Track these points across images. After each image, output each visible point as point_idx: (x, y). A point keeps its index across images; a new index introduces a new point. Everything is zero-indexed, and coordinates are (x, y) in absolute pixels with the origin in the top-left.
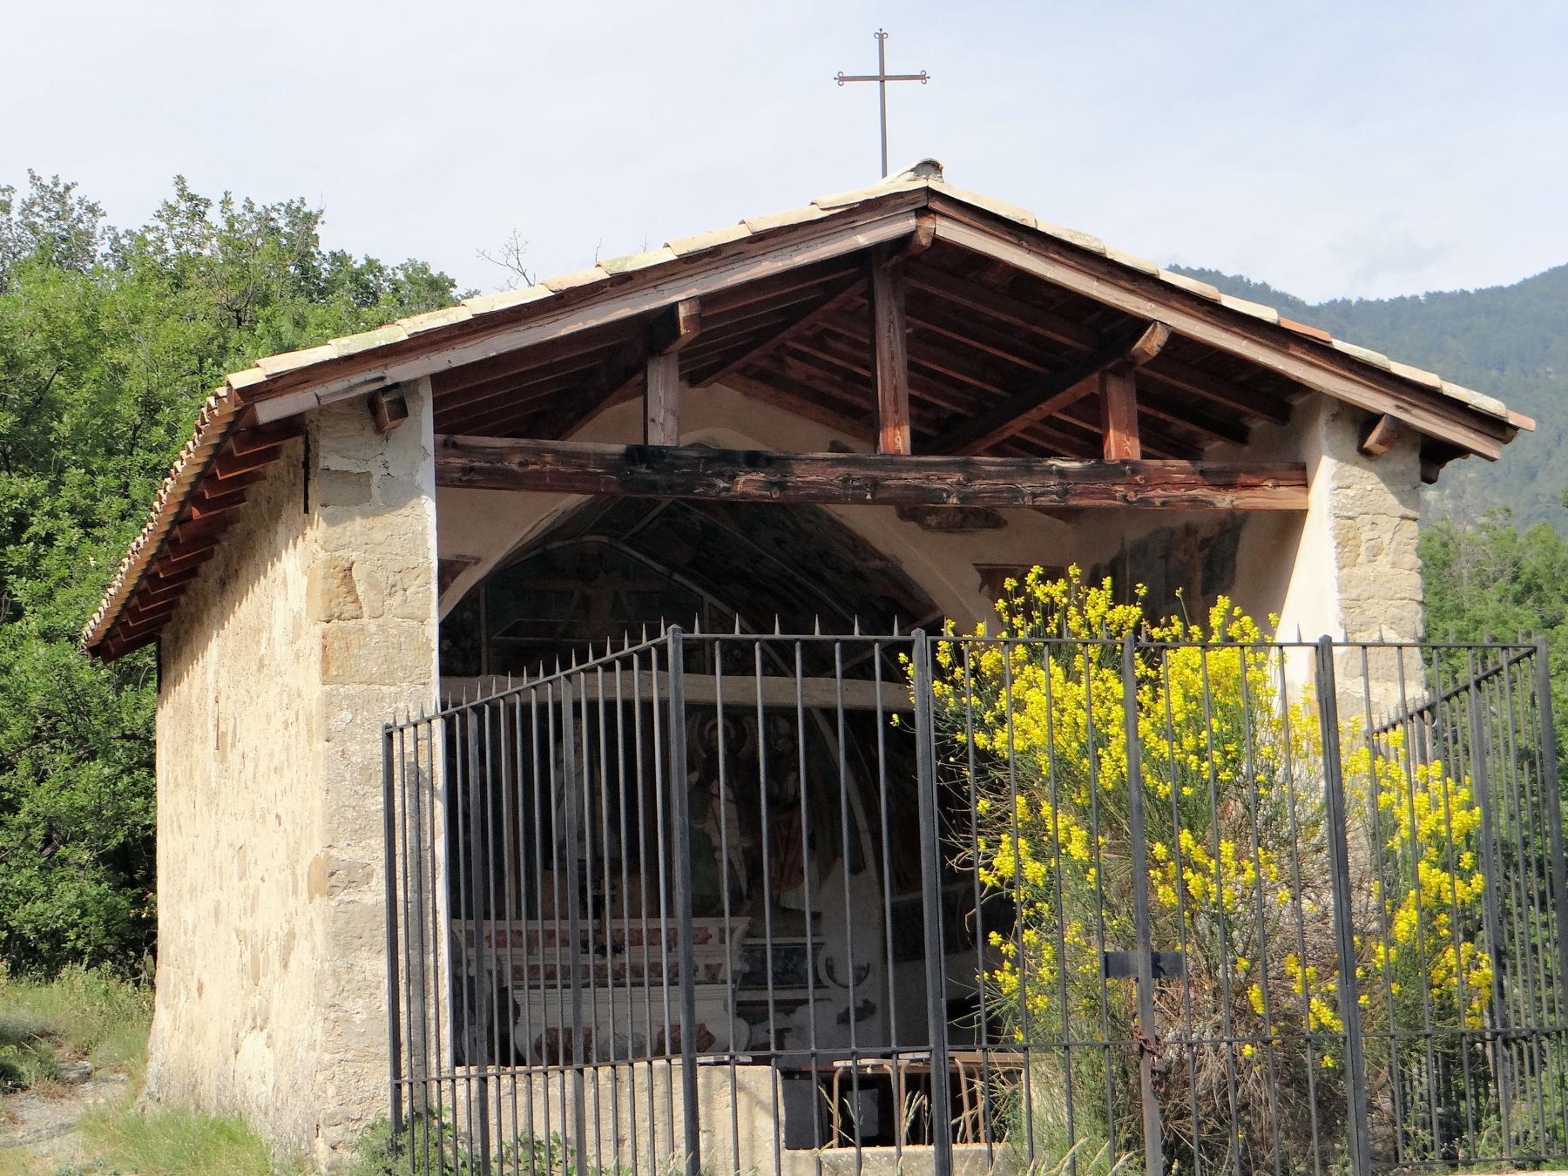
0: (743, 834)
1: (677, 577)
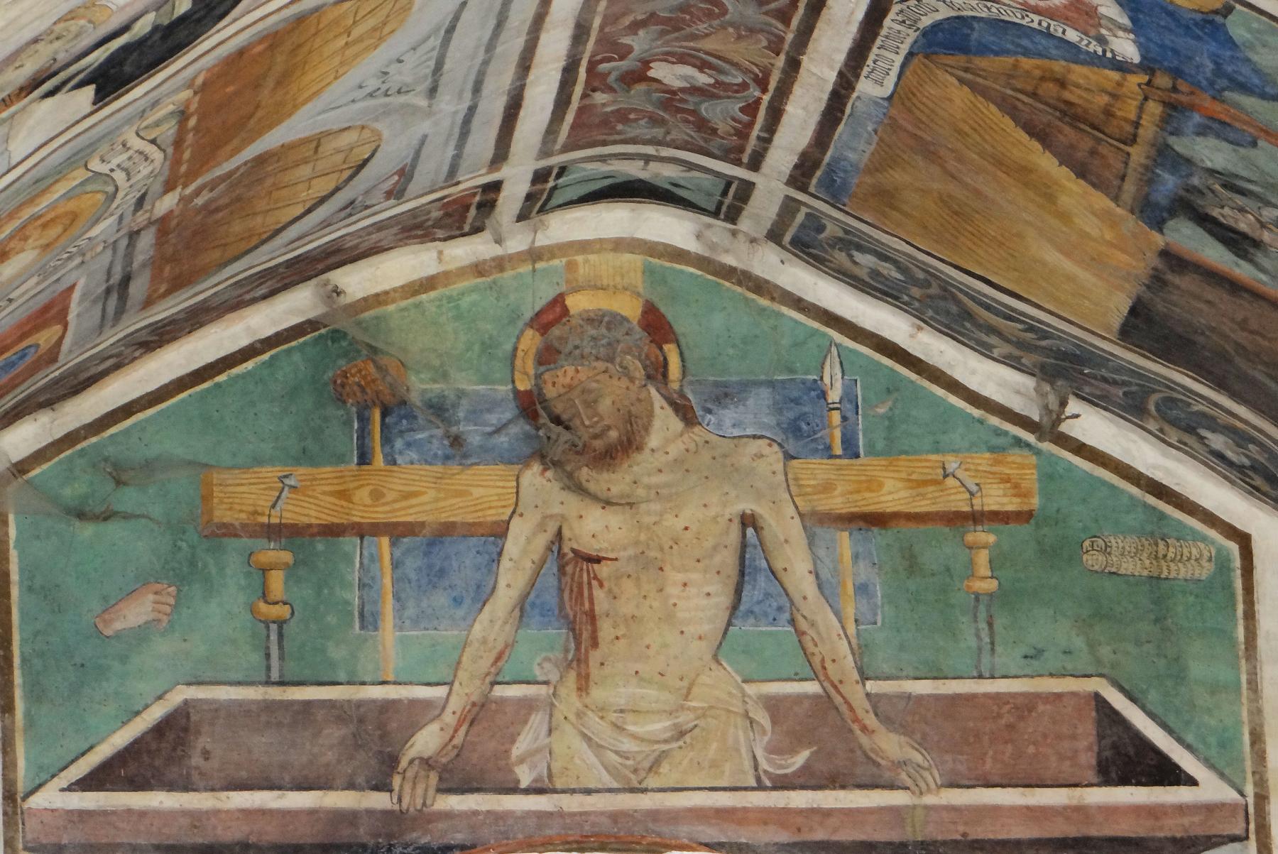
1: (1092, 425)
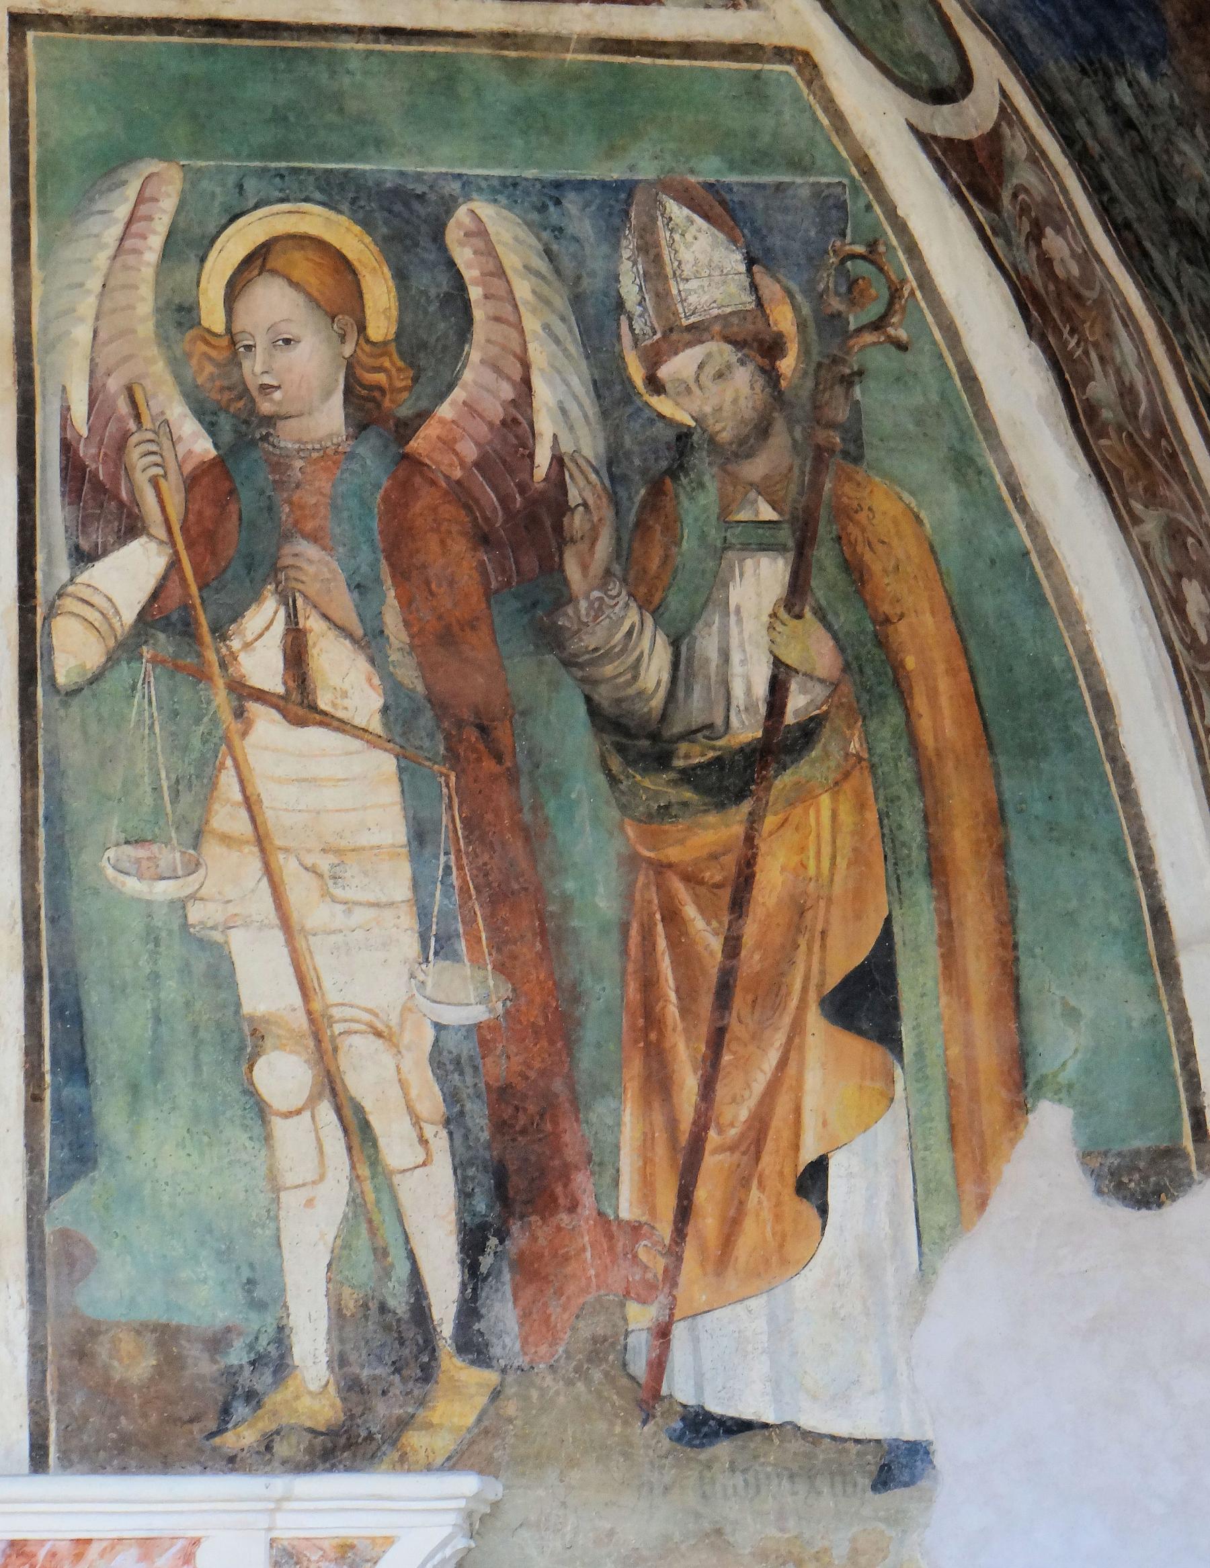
0: (437, 943)
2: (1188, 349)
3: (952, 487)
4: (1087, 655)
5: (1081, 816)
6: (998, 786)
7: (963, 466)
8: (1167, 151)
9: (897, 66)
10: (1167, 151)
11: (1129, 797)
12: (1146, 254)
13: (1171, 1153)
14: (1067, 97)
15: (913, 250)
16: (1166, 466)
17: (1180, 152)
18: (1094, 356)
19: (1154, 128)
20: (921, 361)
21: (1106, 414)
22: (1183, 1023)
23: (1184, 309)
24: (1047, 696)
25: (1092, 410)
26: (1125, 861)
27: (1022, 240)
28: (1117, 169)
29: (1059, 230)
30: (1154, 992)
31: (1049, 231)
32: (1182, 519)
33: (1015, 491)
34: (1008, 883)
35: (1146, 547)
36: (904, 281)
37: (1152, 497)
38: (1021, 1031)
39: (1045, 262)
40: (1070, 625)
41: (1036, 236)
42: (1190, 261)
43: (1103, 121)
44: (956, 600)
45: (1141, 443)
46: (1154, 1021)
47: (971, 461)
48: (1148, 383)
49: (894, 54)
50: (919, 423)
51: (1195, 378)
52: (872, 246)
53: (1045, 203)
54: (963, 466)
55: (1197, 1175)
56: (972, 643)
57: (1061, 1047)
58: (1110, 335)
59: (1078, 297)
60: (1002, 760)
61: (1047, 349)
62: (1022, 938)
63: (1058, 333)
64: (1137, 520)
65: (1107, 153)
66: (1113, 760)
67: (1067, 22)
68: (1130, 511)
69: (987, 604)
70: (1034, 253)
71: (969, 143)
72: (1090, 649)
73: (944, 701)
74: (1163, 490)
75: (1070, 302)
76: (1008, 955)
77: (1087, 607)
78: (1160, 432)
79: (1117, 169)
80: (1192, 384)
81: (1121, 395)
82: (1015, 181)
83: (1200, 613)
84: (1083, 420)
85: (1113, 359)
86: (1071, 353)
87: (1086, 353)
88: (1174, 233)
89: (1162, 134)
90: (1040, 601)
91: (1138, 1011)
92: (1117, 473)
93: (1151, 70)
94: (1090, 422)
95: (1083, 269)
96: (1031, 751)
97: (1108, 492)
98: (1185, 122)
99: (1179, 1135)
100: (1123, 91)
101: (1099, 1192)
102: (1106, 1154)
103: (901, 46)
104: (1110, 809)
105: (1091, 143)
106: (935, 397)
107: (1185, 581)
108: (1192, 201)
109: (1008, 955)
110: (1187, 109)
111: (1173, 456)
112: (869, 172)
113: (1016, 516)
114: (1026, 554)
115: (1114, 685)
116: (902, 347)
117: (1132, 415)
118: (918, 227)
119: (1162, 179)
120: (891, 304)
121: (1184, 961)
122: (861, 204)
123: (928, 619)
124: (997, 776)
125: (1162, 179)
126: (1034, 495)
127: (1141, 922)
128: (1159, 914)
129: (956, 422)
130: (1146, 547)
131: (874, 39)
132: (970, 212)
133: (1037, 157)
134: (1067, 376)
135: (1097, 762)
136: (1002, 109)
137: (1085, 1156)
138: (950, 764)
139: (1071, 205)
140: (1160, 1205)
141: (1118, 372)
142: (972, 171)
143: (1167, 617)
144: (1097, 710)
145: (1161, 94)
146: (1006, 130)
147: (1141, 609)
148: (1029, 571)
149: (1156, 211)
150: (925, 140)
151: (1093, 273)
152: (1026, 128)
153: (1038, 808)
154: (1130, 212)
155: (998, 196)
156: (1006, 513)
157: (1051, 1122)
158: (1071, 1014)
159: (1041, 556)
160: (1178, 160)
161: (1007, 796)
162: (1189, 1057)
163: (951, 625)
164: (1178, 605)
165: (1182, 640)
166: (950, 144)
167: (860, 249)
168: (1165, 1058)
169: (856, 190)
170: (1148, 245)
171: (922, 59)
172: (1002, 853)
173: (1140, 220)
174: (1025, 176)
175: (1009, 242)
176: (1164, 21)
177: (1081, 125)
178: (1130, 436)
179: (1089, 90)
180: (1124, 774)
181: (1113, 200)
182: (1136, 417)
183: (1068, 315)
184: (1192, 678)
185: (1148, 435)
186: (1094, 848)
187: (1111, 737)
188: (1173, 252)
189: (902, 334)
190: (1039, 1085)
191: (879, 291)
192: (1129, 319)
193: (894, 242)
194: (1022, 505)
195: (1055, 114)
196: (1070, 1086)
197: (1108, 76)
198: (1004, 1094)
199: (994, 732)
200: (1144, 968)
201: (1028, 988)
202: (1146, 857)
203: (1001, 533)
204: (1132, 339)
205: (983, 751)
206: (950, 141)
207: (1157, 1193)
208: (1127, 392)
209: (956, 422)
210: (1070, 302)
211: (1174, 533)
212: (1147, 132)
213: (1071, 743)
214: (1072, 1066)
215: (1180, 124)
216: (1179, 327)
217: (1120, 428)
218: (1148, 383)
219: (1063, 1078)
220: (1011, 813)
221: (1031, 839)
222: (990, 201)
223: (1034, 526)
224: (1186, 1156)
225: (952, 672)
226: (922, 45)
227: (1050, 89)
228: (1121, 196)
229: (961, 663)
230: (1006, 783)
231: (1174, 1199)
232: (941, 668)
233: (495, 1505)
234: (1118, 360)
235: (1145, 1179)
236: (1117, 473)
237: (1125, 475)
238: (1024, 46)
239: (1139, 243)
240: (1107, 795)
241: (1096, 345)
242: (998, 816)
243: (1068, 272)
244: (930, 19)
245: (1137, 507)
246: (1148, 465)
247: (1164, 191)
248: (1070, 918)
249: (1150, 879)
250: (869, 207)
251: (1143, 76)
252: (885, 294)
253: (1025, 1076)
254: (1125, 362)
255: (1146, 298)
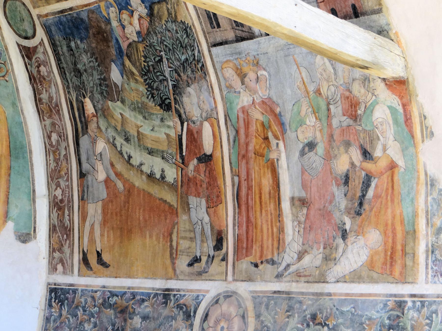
2: (69, 92)
3: (12, 108)
4: (29, 143)
5: (24, 171)
6: (11, 163)
7: (14, 104)
8: (79, 56)
9: (18, 31)
10: (79, 56)
11: (32, 169)
12: (65, 74)
13: (29, 234)
14: (58, 43)
15: (11, 64)
16: (56, 112)
17: (82, 57)
18: (44, 90)
19: (77, 52)
20: (9, 84)
21: (44, 101)
22: (35, 211)
23: (71, 85)
24: (21, 148)
25: (40, 100)
26: (29, 181)
27: (34, 67)
28: (65, 58)
29: (45, 66)
30: (31, 205)
31: (42, 66)
32: (56, 122)
33: (22, 111)
34: (9, 180)
35: (45, 126)
36: (9, 70)
37: (50, 117)
38: (8, 208)
39: (39, 72)
40: (27, 137)
41: (38, 66)
42: (76, 76)
43: (65, 49)
44: (9, 128)
45: (51, 107)
46: (30, 210)
47: (15, 104)
48: (57, 96)
49: (18, 29)
50: (8, 95)
51: (69, 98)
52: (5, 62)
53: (43, 61)
54: (14, 104)
55: (33, 239)
56: (10, 137)
57: (14, 212)
58: (50, 87)
59: (44, 79)
60: (12, 158)
61: (33, 87)
62: (10, 191)
63: (37, 84)
64: (44, 120)
65: (64, 54)
66: (31, 162)
67: (64, 29)
68: (43, 119)
69: (14, 130)
70: (37, 69)
71: (29, 48)
72: (30, 142)
73: (4, 146)
74: (53, 116)
75: (42, 79)
76: (7, 194)
77: (31, 134)
78: (57, 105)
79: (65, 58)
80: (68, 98)
81: (49, 98)
82: (37, 56)
83: (55, 139)
84: (38, 101)
85: (49, 91)
86: (39, 89)
87: (43, 89)
88: (74, 71)
89: (79, 53)
90: (23, 132)
91: (28, 208)
92: (43, 112)
93: (81, 41)
94: (39, 101)
95: (48, 74)
96: (17, 158)
97: (39, 114)
98: (86, 52)
99: (31, 231)
100: (73, 44)
101: (16, 239)
102: (18, 232)
103: (21, 28)
104: (29, 171)
105: (60, 52)
106: (11, 91)
107: (53, 133)
108: (81, 66)
109: (7, 194)
110: (87, 49)
111: (59, 111)
112: (7, 49)
113: (22, 115)
114: (22, 123)
115: (33, 149)
116: (7, 81)
117: (51, 102)
118: (13, 60)
119: (75, 61)
120: (6, 73)
121: (37, 200)
122: (4, 54)
123: (4, 131)
124: (11, 161)
125: (75, 61)
126: (25, 112)
127: (30, 192)
128: (34, 191)
129: (14, 96)
130: (45, 126)
131: (15, 25)
132: (24, 60)
133: (45, 52)
134: (36, 93)
135: (28, 162)
136: (40, 43)
137: (15, 232)
138: (3, 158)
139: (50, 62)
140: (26, 243)
141: (50, 94)
142: (28, 53)
143: (46, 139)
144: (29, 152)
145: (82, 46)
146: (39, 46)
147: (40, 136)
148: (21, 125)
149: (71, 66)
150: (18, 45)
151: (50, 75)
152: (44, 47)
153: (17, 168)
154: (65, 66)
155: (32, 58)
156: (20, 114)
157: (10, 225)
158: (17, 206)
159: (24, 123)
160: (81, 58)
161: (12, 165)
162: (35, 217)
163: (7, 133)
164: (49, 137)
165: (48, 143)
166: (24, 47)
167: (3, 62)
168: (30, 217)
169: (4, 51)
170: (66, 72)
171: (25, 31)
172: (9, 175)
173: (67, 67)
174: (40, 56)
175: (31, 66)
176: (89, 33)
177: (59, 48)
178: (49, 105)
179: (64, 42)
180: (32, 165)
181: (61, 63)
182: (51, 102)
183: (40, 82)
184: (49, 150)
185: (53, 106)
186: (25, 177)
187: (31, 158)
188: (72, 75)
189: (7, 79)
190: (9, 218)
191: (5, 70)
192: (56, 85)
193: (9, 62)
194: (23, 114)
195: (54, 45)
196: (14, 219)
197: (70, 40)
198: (3, 219)
199: (11, 153)
200: (30, 200)
201: (10, 200)
202: (33, 181)
203: (19, 118)
204: (55, 88)
205: (9, 156)
206: (25, 46)
207: (26, 241)
208: (51, 98)
209: (14, 96)
210: (42, 79)
211: (53, 124)
212: (75, 52)
213: (24, 158)
214: (15, 216)
215: (84, 52)
216: (68, 87)
217: (47, 104)
218: (57, 96)
219: (13, 218)
220: (12, 168)
221: (15, 173)
222: (30, 58)
223: (24, 118)
224: (31, 235)
225: (6, 141)
226: (27, 28)
227: (54, 41)
228: (64, 62)
229: (8, 140)
230: (12, 163)
231: (28, 242)
232: (4, 140)
233: (279, 218)
234: (50, 91)
235: (24, 238)
236: (43, 112)
237: (45, 112)
238: (52, 32)
239: (65, 72)
240: (29, 168)
241: (46, 88)
242: (10, 168)
243: (44, 74)
244: (31, 24)
245: (45, 118)
246: (51, 111)
247: (75, 63)
248: (19, 189)
249: (33, 184)
250: (6, 55)
251: (79, 42)
252: (6, 71)
253: (7, 216)
254: (52, 92)
255: (62, 82)
